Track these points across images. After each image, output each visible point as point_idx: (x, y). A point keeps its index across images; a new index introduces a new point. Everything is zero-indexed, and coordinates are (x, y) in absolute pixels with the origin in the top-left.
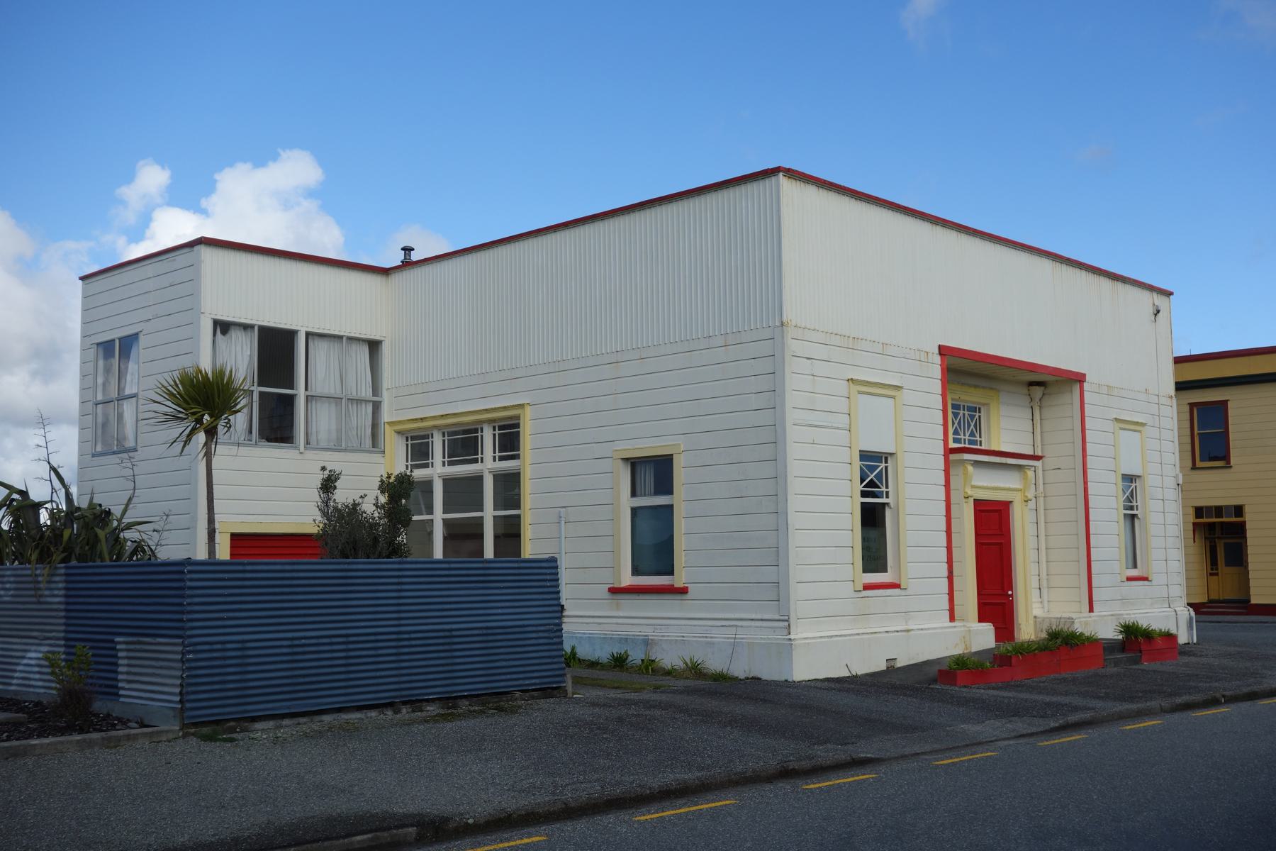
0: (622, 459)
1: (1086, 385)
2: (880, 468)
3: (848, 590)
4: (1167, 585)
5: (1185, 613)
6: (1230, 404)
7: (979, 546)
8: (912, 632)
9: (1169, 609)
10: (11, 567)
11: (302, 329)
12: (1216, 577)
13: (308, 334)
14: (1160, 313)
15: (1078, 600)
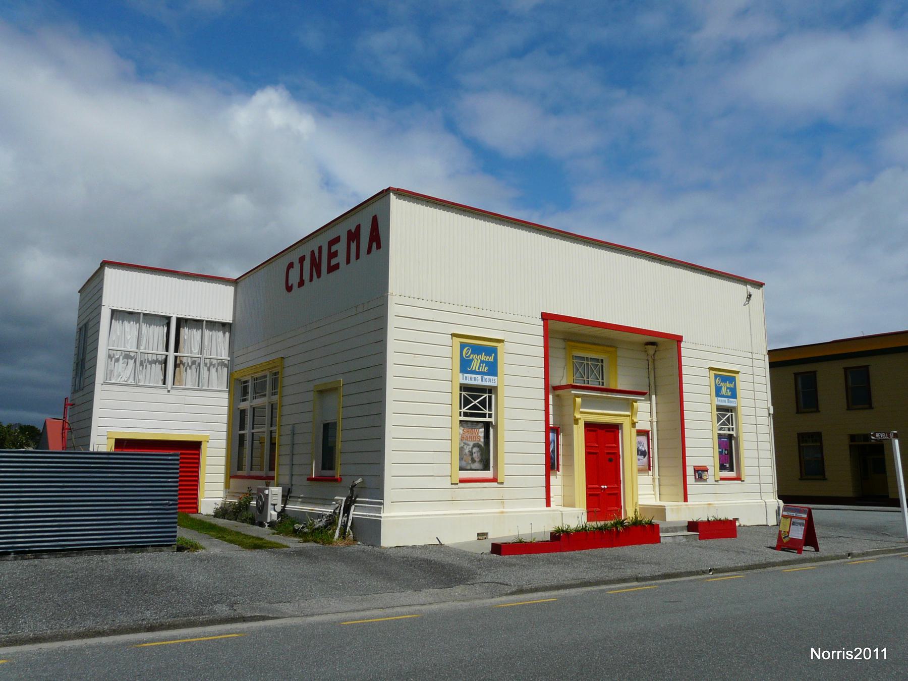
0: (317, 391)
1: (683, 345)
2: (728, 415)
3: (447, 482)
4: (760, 484)
5: (774, 502)
6: (871, 369)
7: (588, 454)
8: (505, 514)
9: (761, 501)
10: (7, 453)
11: (173, 316)
12: (716, 480)
13: (179, 320)
14: (752, 297)
15: (653, 493)
